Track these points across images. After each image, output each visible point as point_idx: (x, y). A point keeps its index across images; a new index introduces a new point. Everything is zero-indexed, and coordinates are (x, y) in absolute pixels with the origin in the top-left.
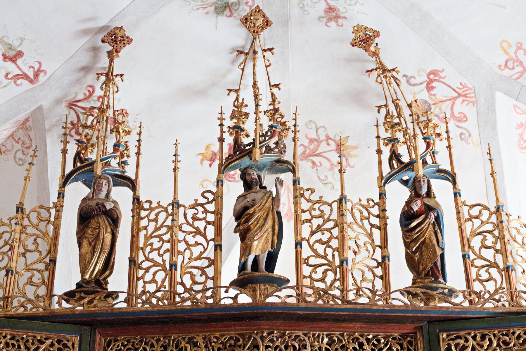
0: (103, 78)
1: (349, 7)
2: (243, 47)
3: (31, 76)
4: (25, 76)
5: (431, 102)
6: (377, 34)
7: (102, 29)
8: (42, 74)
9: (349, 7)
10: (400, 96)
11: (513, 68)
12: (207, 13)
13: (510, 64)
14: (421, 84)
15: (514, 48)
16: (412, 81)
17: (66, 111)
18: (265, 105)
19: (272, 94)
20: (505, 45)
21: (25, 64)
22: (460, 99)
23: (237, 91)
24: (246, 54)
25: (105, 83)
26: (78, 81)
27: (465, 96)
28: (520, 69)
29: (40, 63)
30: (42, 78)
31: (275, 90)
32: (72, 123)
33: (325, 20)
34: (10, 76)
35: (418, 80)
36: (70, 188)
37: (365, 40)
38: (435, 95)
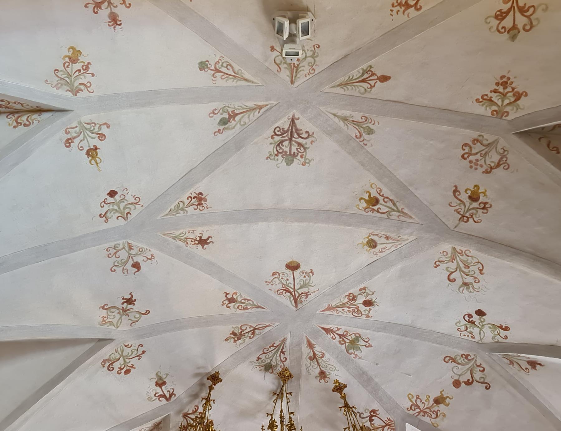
0: (204, 401)
1: (331, 372)
2: (276, 391)
3: (168, 397)
4: (164, 396)
5: (372, 428)
6: (345, 386)
7: (207, 374)
8: (173, 396)
9: (331, 372)
10: (356, 422)
11: (415, 410)
12: (261, 370)
13: (413, 408)
14: (367, 417)
15: (415, 398)
16: (362, 415)
17: (182, 419)
18: (286, 422)
19: (290, 418)
20: (410, 396)
21: (166, 389)
22: (387, 427)
23: (271, 415)
24: (278, 394)
25: (205, 404)
26: (190, 402)
27: (390, 425)
28: (418, 410)
29: (173, 390)
30: (173, 398)
31: (291, 415)
32: (184, 426)
33: (319, 378)
34: (157, 395)
35: (365, 415)
36: (363, 89)
37: (339, 388)
38: (373, 424)
